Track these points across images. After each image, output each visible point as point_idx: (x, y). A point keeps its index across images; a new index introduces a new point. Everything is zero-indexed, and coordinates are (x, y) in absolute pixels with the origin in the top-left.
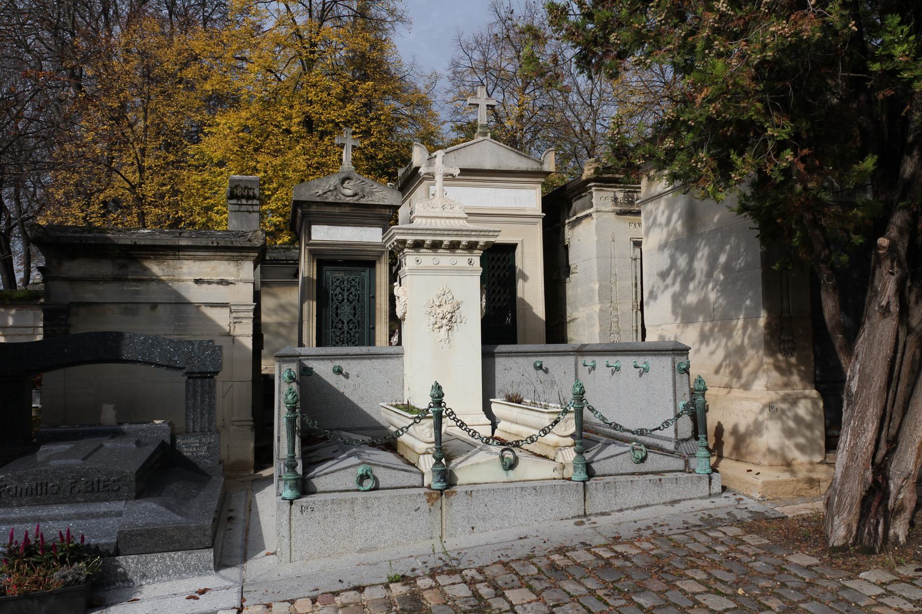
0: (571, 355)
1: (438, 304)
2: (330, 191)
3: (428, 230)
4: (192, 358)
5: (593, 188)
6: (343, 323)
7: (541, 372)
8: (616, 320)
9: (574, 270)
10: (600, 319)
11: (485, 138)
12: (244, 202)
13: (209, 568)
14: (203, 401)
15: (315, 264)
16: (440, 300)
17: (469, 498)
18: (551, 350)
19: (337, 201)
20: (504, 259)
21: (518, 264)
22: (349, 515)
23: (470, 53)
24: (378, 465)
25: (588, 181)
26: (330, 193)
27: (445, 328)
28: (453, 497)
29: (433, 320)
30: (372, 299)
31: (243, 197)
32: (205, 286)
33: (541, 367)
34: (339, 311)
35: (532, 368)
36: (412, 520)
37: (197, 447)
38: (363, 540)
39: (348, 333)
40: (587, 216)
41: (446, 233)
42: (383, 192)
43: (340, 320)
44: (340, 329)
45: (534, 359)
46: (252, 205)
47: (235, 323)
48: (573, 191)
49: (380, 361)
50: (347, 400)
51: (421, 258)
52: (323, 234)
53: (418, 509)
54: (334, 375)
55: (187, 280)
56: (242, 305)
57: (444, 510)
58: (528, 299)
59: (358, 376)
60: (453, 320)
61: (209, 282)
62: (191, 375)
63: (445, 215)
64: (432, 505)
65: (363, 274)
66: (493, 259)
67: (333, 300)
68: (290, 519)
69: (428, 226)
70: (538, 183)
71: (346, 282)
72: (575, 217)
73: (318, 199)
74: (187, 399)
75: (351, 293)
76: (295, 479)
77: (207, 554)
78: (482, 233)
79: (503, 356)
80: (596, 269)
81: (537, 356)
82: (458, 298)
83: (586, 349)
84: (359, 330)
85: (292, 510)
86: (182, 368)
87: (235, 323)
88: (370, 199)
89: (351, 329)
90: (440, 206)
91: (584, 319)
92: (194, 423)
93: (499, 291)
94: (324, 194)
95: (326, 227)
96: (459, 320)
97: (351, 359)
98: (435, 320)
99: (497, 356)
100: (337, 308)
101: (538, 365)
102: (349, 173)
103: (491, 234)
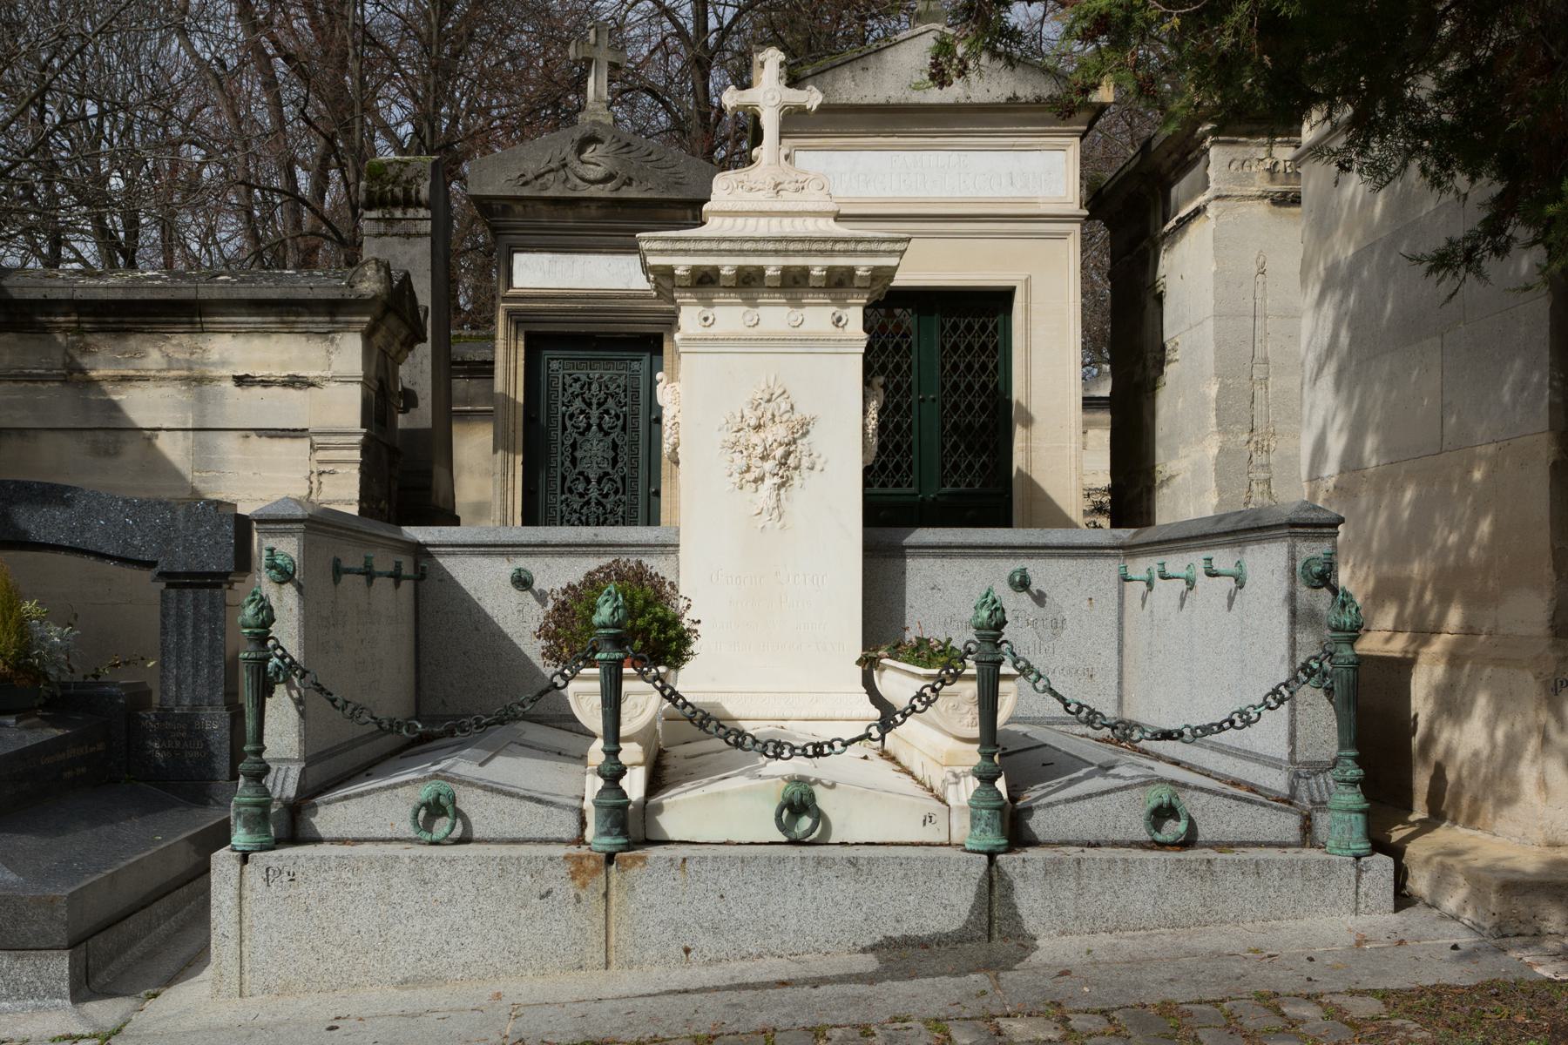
0: (1108, 556)
1: (753, 422)
2: (552, 170)
3: (724, 240)
4: (172, 540)
6: (588, 481)
7: (1025, 596)
8: (1263, 475)
13: (59, 995)
14: (197, 639)
15: (521, 343)
16: (759, 413)
17: (679, 875)
20: (984, 328)
22: (379, 896)
24: (470, 784)
26: (551, 176)
27: (770, 482)
28: (635, 871)
29: (740, 461)
30: (655, 426)
32: (257, 390)
34: (578, 454)
36: (531, 918)
37: (181, 740)
38: (411, 959)
39: (599, 503)
44: (581, 495)
47: (320, 474)
53: (549, 893)
54: (514, 590)
55: (220, 379)
56: (336, 434)
57: (614, 900)
60: (791, 461)
61: (266, 383)
62: (173, 580)
63: (779, 207)
64: (584, 885)
65: (635, 365)
66: (955, 327)
67: (564, 428)
68: (241, 897)
69: (747, 233)
70: (1072, 134)
71: (595, 386)
73: (526, 192)
74: (164, 630)
75: (607, 412)
76: (256, 805)
77: (56, 961)
79: (929, 555)
80: (1212, 347)
81: (1016, 556)
82: (803, 410)
84: (624, 498)
85: (246, 876)
86: (150, 565)
87: (320, 474)
89: (606, 496)
91: (1189, 474)
92: (178, 685)
96: (805, 463)
97: (553, 554)
98: (744, 462)
99: (913, 556)
100: (574, 446)
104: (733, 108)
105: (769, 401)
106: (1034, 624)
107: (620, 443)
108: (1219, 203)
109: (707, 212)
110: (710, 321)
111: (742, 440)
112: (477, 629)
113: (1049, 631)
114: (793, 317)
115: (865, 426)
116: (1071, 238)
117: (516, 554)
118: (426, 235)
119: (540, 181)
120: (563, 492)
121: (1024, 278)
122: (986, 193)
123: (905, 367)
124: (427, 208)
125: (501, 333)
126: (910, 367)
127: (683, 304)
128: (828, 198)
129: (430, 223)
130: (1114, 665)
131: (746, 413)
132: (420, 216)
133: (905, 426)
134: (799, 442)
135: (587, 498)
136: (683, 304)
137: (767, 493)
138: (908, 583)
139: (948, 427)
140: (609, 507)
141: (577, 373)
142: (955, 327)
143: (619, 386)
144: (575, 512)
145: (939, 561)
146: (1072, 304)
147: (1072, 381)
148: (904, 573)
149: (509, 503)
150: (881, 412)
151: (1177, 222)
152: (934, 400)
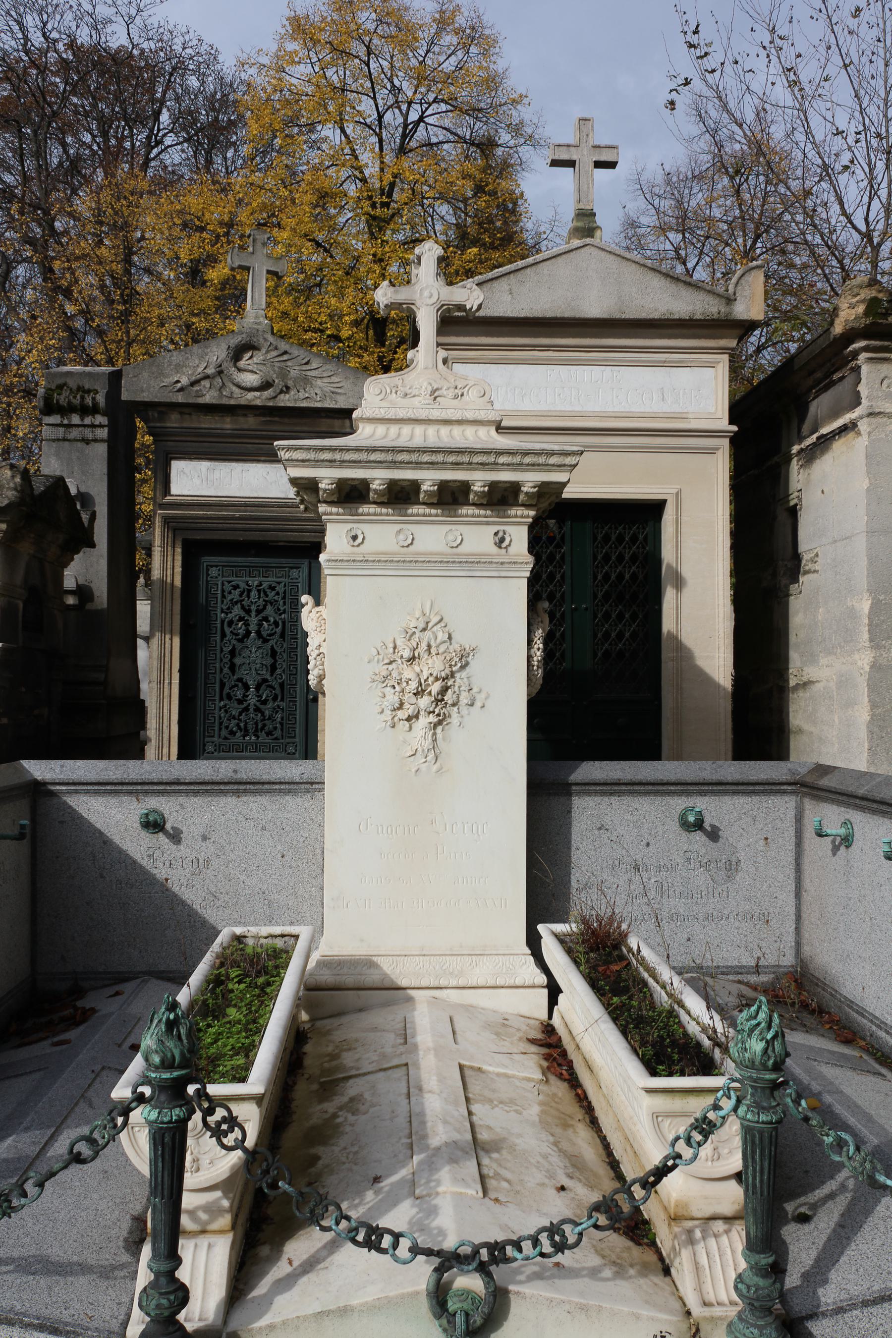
0: (784, 792)
1: (407, 654)
2: (207, 377)
5: (863, 356)
6: (247, 687)
9: (810, 566)
10: (873, 688)
11: (588, 240)
12: (76, 419)
15: (179, 550)
18: (730, 779)
19: (225, 401)
20: (634, 539)
21: (668, 554)
23: (656, 202)
25: (850, 336)
26: (206, 383)
27: (425, 721)
29: (392, 698)
31: (71, 409)
33: (699, 825)
34: (238, 661)
35: (674, 825)
40: (843, 430)
41: (426, 458)
42: (334, 379)
43: (240, 680)
44: (240, 702)
45: (679, 804)
46: (93, 426)
48: (811, 373)
49: (263, 800)
50: (175, 902)
51: (360, 529)
52: (197, 481)
54: (144, 834)
58: (688, 638)
59: (205, 838)
60: (449, 697)
63: (436, 414)
65: (294, 573)
66: (606, 538)
67: (223, 635)
69: (402, 442)
70: (722, 350)
71: (254, 593)
72: (815, 436)
73: (180, 398)
75: (266, 619)
78: (527, 460)
79: (596, 793)
80: (864, 563)
81: (688, 794)
82: (462, 640)
83: (826, 782)
88: (302, 395)
89: (264, 702)
90: (426, 388)
91: (832, 684)
93: (620, 616)
94: (193, 384)
95: (204, 465)
96: (464, 699)
97: (187, 793)
99: (579, 794)
100: (233, 653)
101: (691, 819)
102: (254, 333)
103: (553, 460)
104: (386, 306)
105: (424, 630)
106: (705, 866)
107: (278, 650)
108: (873, 420)
109: (356, 419)
110: (359, 540)
111: (395, 674)
112: (102, 876)
113: (723, 873)
114: (451, 537)
115: (529, 658)
116: (720, 453)
117: (146, 793)
118: (102, 441)
119: (196, 388)
120: (221, 699)
121: (675, 491)
122: (637, 408)
123: (558, 577)
124: (103, 415)
125: (157, 541)
126: (563, 577)
127: (330, 521)
128: (489, 406)
129: (106, 429)
130: (792, 910)
131: (398, 643)
132: (97, 423)
133: (558, 635)
134: (457, 675)
135: (245, 704)
136: (330, 521)
137: (422, 733)
138: (574, 823)
139: (600, 635)
140: (267, 713)
141: (236, 581)
142: (606, 538)
143: (278, 594)
144: (234, 718)
145: (606, 799)
146: (720, 517)
147: (721, 593)
148: (569, 812)
149: (165, 711)
150: (547, 640)
151: (818, 438)
152: (586, 609)
